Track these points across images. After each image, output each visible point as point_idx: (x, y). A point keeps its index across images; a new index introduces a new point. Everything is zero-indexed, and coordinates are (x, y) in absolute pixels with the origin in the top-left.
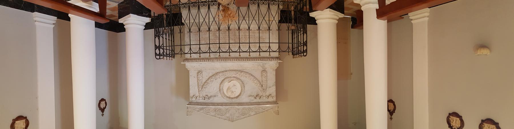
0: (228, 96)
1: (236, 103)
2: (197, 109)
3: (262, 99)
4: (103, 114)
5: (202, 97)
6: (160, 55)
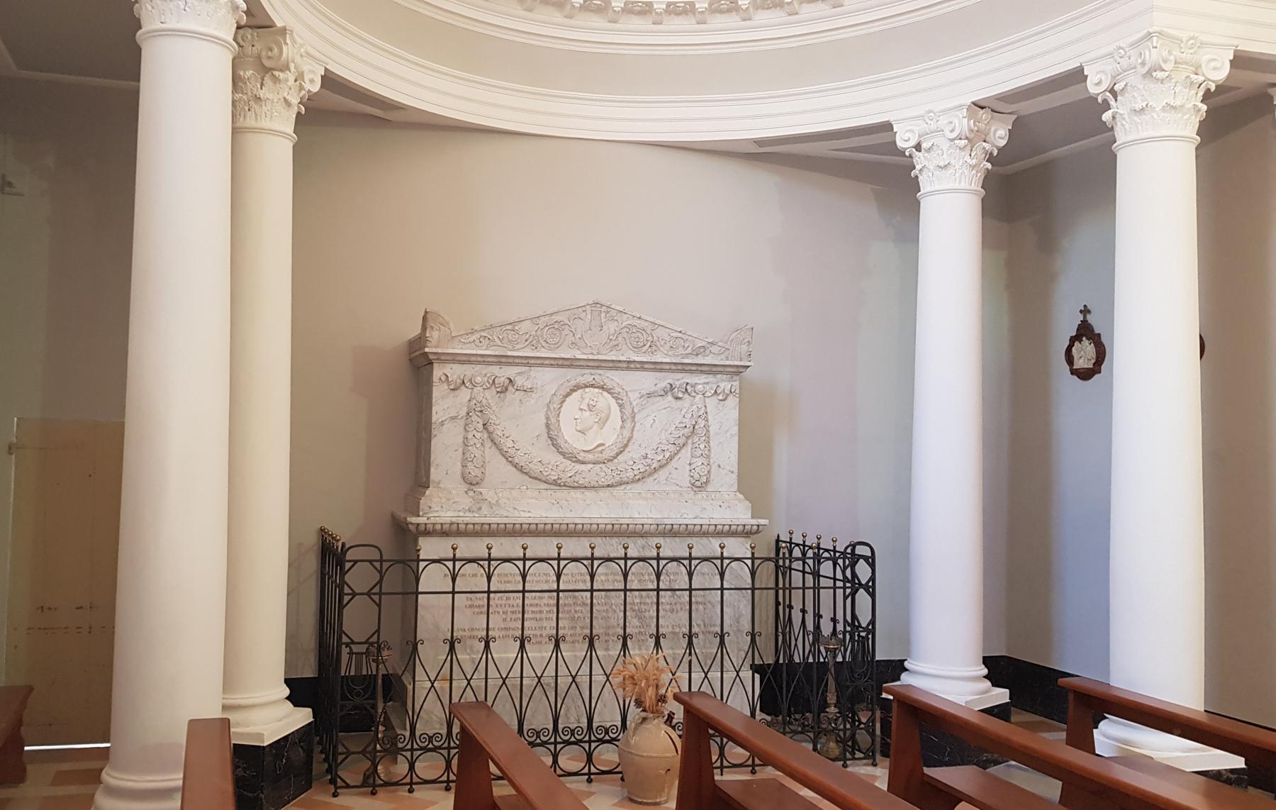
0: (605, 394)
2: (715, 349)
3: (486, 375)
4: (1085, 317)
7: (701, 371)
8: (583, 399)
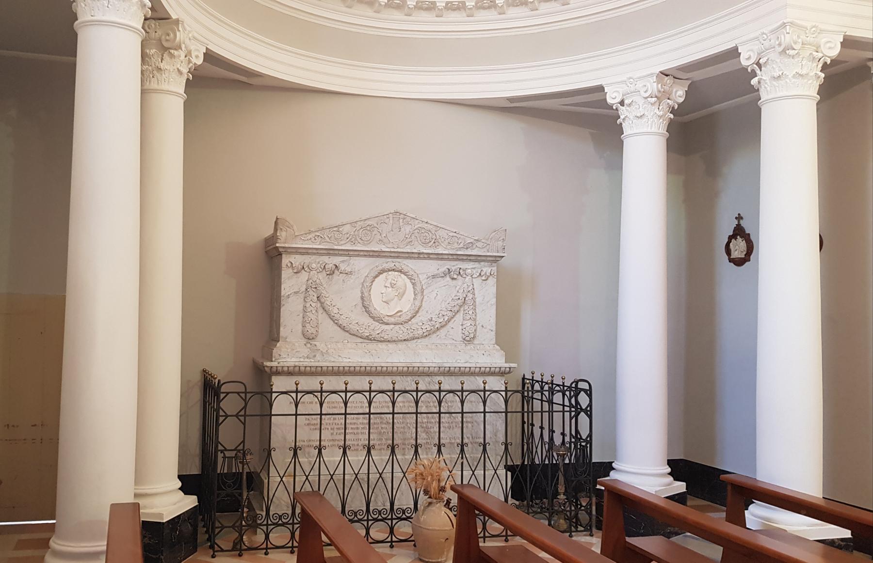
0: (403, 275)
2: (479, 244)
4: (739, 222)
8: (387, 279)
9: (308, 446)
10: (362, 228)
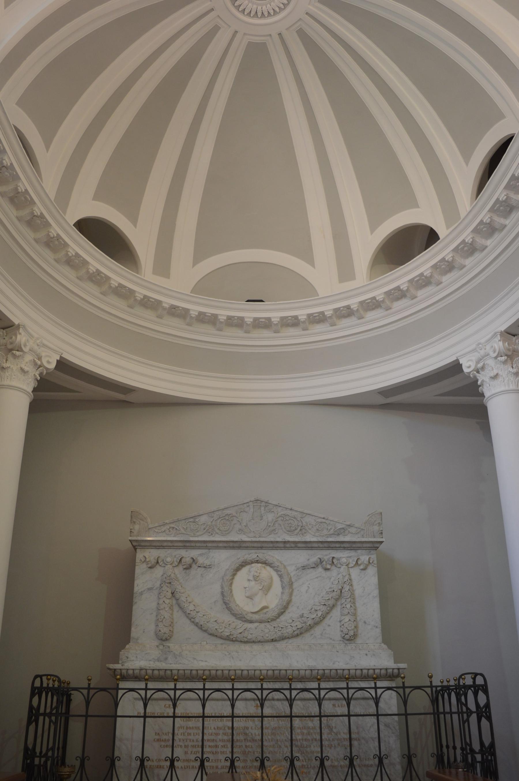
0: (268, 568)
1: (247, 548)
2: (353, 530)
3: (175, 556)
5: (339, 565)
6: (476, 689)
7: (344, 547)
8: (250, 572)
9: (158, 767)
10: (220, 518)
